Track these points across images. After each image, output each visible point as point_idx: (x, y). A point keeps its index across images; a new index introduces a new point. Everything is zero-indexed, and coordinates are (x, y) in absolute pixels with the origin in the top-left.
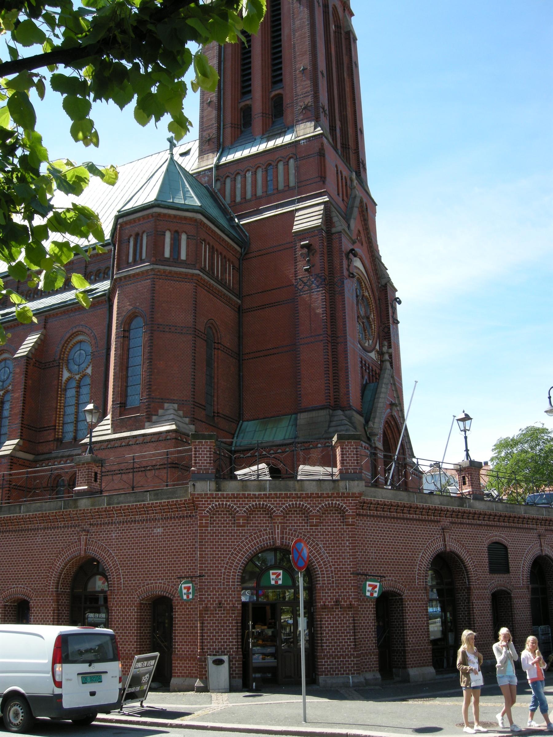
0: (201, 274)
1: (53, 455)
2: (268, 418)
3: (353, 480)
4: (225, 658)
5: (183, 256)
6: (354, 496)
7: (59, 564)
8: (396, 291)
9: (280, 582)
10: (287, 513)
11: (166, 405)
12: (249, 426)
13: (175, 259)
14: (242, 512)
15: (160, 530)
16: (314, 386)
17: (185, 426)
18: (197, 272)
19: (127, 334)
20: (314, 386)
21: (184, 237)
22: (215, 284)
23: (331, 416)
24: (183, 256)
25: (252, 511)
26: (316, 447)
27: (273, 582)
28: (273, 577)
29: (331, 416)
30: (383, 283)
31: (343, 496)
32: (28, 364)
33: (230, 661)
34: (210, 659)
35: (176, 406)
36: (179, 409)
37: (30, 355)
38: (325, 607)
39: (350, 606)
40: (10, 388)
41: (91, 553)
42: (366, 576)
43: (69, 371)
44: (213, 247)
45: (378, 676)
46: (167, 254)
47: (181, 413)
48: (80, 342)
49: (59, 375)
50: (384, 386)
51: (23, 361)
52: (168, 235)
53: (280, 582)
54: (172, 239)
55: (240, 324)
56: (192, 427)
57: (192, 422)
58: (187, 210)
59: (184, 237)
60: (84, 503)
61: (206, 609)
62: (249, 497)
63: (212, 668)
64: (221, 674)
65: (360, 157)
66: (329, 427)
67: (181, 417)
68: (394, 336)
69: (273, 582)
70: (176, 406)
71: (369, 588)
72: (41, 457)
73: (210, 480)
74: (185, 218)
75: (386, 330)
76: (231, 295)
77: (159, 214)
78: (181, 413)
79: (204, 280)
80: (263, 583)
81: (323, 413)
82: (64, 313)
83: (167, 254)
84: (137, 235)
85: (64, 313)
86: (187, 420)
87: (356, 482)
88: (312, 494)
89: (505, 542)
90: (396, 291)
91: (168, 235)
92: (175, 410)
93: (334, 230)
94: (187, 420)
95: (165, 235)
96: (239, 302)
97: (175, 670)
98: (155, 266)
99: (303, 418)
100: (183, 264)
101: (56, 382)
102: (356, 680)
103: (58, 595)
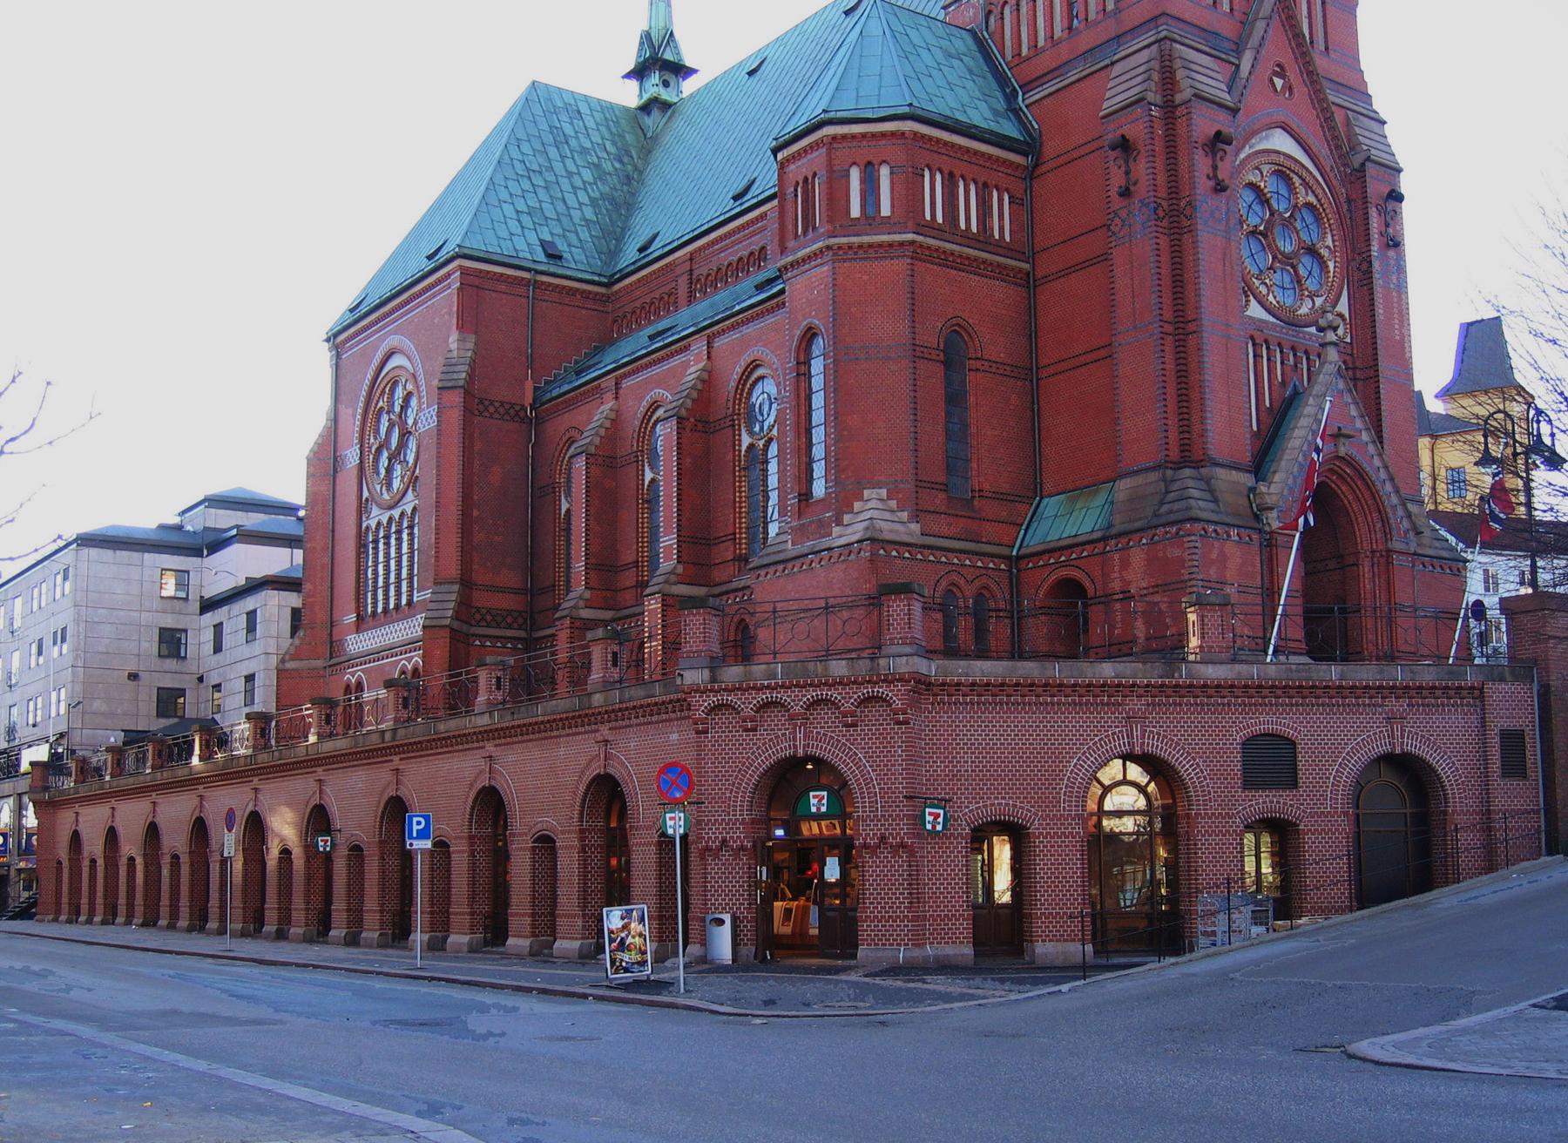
0: (920, 238)
1: (734, 585)
2: (1079, 488)
4: (727, 918)
5: (886, 211)
8: (1399, 171)
9: (824, 809)
11: (866, 493)
12: (1051, 505)
13: (870, 219)
16: (1143, 423)
17: (898, 527)
19: (803, 369)
20: (1143, 423)
21: (884, 171)
23: (1168, 482)
24: (886, 211)
27: (814, 809)
28: (813, 801)
29: (1168, 482)
30: (1357, 161)
31: (889, 680)
36: (889, 498)
38: (865, 846)
39: (902, 845)
41: (611, 771)
42: (928, 801)
43: (751, 433)
44: (951, 174)
46: (855, 212)
47: (893, 504)
48: (762, 378)
49: (736, 442)
50: (1311, 401)
52: (855, 174)
53: (824, 809)
54: (863, 181)
55: (1031, 310)
57: (915, 517)
59: (884, 171)
65: (152, 536)
66: (1162, 503)
67: (892, 511)
68: (1386, 275)
70: (883, 493)
71: (929, 818)
74: (883, 135)
75: (1364, 266)
77: (834, 138)
78: (893, 504)
80: (801, 811)
81: (1154, 476)
83: (855, 212)
84: (806, 179)
88: (842, 678)
90: (1399, 171)
91: (855, 174)
93: (1178, 98)
94: (904, 515)
95: (848, 176)
97: (862, 935)
99: (1124, 485)
100: (888, 225)
101: (730, 456)
102: (908, 954)
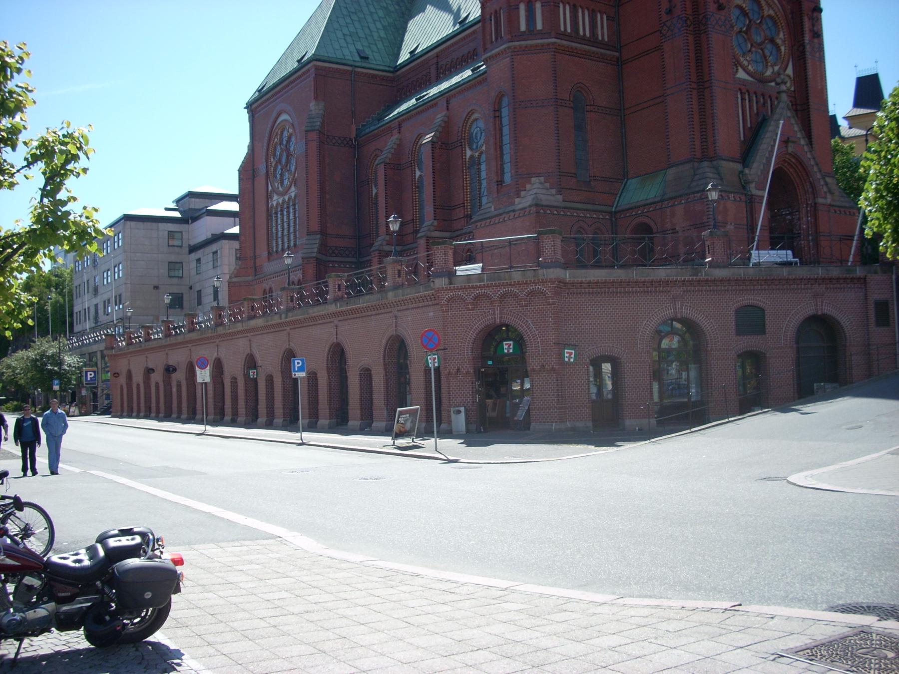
0: (558, 41)
1: (464, 231)
3: (550, 268)
4: (462, 409)
5: (539, 26)
6: (552, 281)
7: (384, 342)
9: (511, 351)
10: (503, 297)
11: (533, 180)
12: (633, 183)
13: (531, 32)
14: (469, 299)
15: (432, 314)
18: (554, 40)
22: (579, 45)
24: (539, 26)
25: (477, 298)
26: (680, 203)
32: (433, 148)
33: (466, 410)
34: (452, 410)
35: (542, 179)
36: (545, 182)
37: (435, 140)
38: (533, 370)
40: (484, 148)
45: (590, 424)
46: (523, 28)
47: (547, 185)
48: (476, 120)
49: (463, 154)
51: (430, 146)
53: (511, 351)
56: (560, 197)
58: (432, 50)
59: (538, 5)
60: (390, 295)
61: (449, 373)
62: (473, 287)
63: (453, 416)
64: (460, 421)
67: (547, 189)
69: (506, 351)
72: (408, 247)
73: (444, 276)
76: (602, 51)
78: (547, 185)
79: (563, 46)
82: (460, 92)
83: (523, 28)
84: (496, 11)
85: (460, 92)
86: (554, 191)
87: (552, 270)
89: (761, 305)
92: (541, 183)
94: (554, 191)
95: (518, 8)
96: (617, 54)
98: (511, 44)
99: (671, 172)
100: (542, 34)
103: (385, 365)
